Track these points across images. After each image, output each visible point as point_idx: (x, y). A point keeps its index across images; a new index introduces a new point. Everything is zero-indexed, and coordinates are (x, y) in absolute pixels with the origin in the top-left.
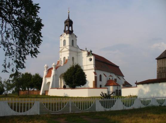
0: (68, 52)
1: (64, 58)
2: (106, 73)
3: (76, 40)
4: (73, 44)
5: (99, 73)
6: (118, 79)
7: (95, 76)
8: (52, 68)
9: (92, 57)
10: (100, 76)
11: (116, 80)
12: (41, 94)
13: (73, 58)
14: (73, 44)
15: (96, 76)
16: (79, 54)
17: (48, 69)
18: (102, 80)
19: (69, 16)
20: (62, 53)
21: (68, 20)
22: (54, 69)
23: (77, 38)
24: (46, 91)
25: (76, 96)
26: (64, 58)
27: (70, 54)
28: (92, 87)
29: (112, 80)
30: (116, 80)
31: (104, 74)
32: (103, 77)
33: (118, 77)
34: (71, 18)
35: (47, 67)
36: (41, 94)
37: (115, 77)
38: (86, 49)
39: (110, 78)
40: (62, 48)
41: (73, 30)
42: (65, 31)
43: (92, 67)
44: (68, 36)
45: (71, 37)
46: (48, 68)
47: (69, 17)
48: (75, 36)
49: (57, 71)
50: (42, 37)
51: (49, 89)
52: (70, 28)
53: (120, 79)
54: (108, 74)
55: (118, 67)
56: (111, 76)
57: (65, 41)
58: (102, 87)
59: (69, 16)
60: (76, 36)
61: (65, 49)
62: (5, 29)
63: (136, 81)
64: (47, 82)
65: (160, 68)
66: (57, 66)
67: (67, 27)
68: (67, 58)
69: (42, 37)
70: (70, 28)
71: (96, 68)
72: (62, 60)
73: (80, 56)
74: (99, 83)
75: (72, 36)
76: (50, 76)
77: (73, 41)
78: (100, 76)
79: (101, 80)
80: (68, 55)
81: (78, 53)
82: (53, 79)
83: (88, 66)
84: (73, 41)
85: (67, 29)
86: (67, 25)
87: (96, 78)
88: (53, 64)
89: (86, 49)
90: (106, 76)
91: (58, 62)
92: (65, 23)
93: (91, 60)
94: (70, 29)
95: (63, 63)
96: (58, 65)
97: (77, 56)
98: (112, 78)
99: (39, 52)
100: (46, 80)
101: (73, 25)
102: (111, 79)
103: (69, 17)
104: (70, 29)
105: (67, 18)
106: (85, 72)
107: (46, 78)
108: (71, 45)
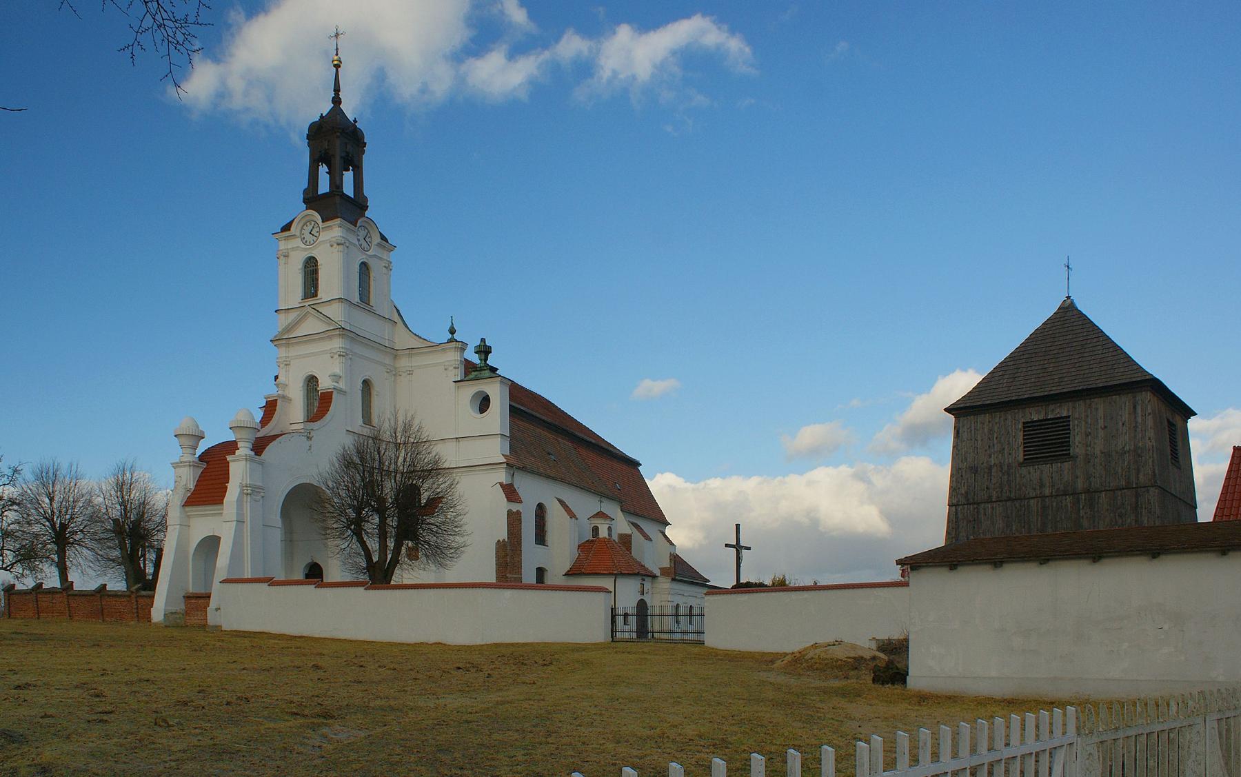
5: (534, 490)
7: (510, 513)
10: (541, 510)
11: (626, 540)
13: (367, 384)
15: (515, 507)
19: (337, 90)
22: (244, 450)
24: (198, 601)
26: (312, 381)
29: (607, 542)
31: (560, 501)
32: (555, 515)
33: (636, 526)
37: (622, 525)
38: (452, 331)
39: (596, 530)
41: (367, 191)
43: (496, 450)
47: (337, 101)
48: (377, 239)
52: (348, 176)
54: (586, 504)
55: (635, 464)
56: (600, 515)
57: (311, 269)
58: (549, 579)
59: (337, 90)
60: (383, 238)
63: (749, 549)
65: (974, 470)
70: (348, 176)
74: (532, 556)
77: (364, 267)
78: (541, 510)
79: (541, 538)
83: (463, 443)
84: (364, 267)
87: (514, 520)
89: (452, 331)
90: (572, 515)
93: (484, 403)
97: (394, 373)
98: (610, 529)
99: (483, 340)
101: (368, 160)
102: (603, 533)
103: (337, 101)
104: (348, 189)
105: (326, 107)
108: (356, 298)
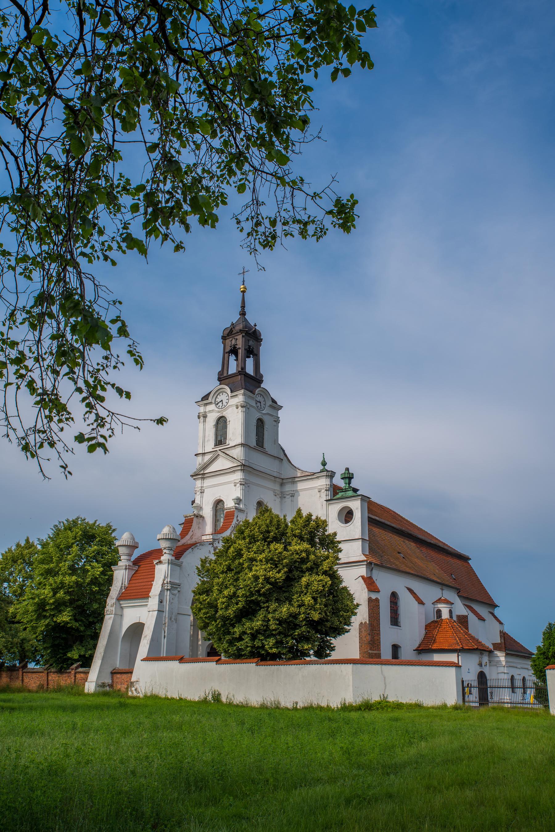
0: (238, 476)
1: (219, 503)
2: (419, 587)
3: (277, 421)
4: (260, 442)
6: (472, 619)
8: (158, 553)
9: (355, 505)
10: (394, 596)
11: (463, 621)
12: (90, 686)
14: (260, 442)
15: (374, 596)
16: (288, 488)
17: (133, 558)
18: (403, 618)
19: (243, 307)
20: (208, 482)
21: (240, 327)
23: (280, 413)
25: (475, 616)
26: (219, 503)
27: (245, 484)
28: (356, 655)
30: (463, 621)
34: (251, 319)
35: (133, 547)
36: (90, 686)
38: (324, 464)
39: (439, 612)
40: (207, 458)
42: (223, 378)
44: (240, 398)
45: (253, 403)
46: (137, 553)
47: (243, 314)
48: (270, 403)
49: (180, 566)
50: (317, 241)
51: (138, 662)
53: (482, 619)
55: (465, 559)
59: (243, 307)
60: (274, 401)
61: (222, 463)
62: (35, 225)
64: (126, 623)
66: (183, 542)
67: (232, 358)
68: (229, 504)
69: (317, 241)
71: (371, 559)
72: (208, 512)
73: (293, 496)
75: (259, 399)
76: (145, 595)
77: (260, 423)
78: (394, 596)
79: (395, 621)
80: (238, 492)
81: (282, 485)
82: (160, 611)
84: (260, 423)
85: (233, 368)
86: (234, 351)
88: (163, 528)
89: (324, 464)
90: (421, 602)
91: (188, 524)
92: (224, 338)
94: (250, 369)
95: (209, 528)
96: (187, 540)
98: (451, 612)
100: (120, 616)
101: (263, 350)
102: (445, 615)
103: (243, 314)
104: (250, 369)
106: (341, 574)
107: (124, 603)
108: (253, 443)
